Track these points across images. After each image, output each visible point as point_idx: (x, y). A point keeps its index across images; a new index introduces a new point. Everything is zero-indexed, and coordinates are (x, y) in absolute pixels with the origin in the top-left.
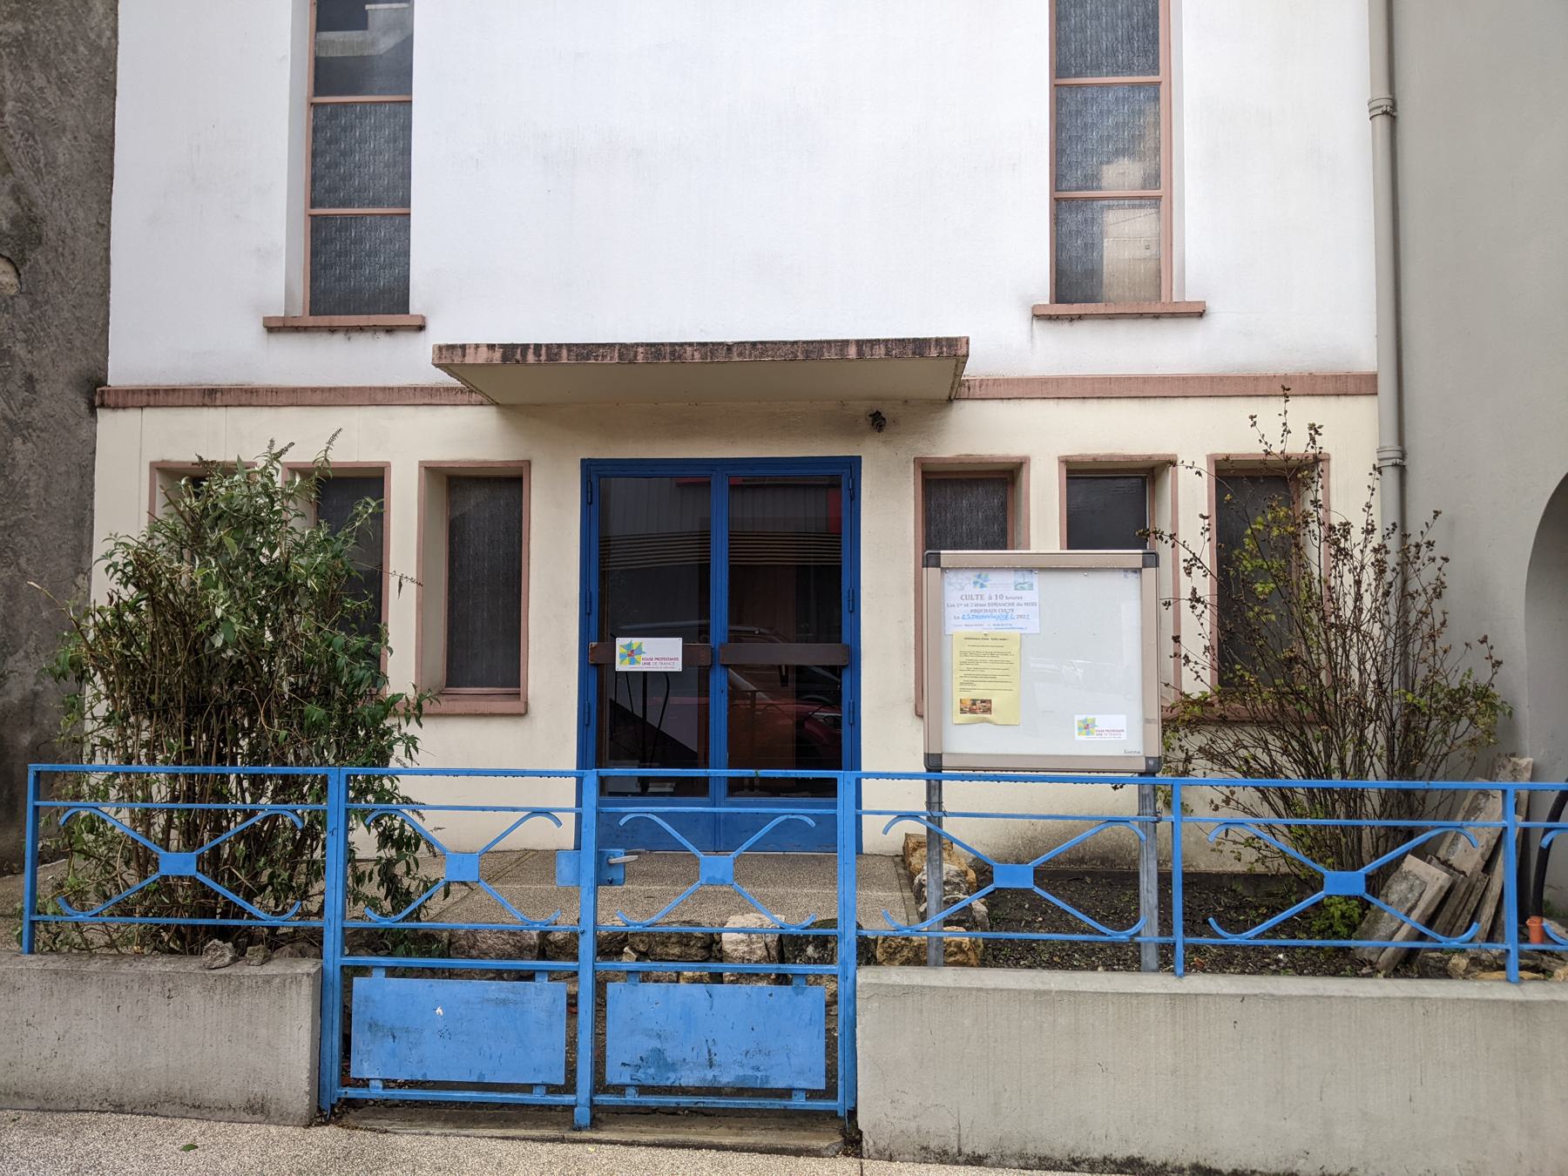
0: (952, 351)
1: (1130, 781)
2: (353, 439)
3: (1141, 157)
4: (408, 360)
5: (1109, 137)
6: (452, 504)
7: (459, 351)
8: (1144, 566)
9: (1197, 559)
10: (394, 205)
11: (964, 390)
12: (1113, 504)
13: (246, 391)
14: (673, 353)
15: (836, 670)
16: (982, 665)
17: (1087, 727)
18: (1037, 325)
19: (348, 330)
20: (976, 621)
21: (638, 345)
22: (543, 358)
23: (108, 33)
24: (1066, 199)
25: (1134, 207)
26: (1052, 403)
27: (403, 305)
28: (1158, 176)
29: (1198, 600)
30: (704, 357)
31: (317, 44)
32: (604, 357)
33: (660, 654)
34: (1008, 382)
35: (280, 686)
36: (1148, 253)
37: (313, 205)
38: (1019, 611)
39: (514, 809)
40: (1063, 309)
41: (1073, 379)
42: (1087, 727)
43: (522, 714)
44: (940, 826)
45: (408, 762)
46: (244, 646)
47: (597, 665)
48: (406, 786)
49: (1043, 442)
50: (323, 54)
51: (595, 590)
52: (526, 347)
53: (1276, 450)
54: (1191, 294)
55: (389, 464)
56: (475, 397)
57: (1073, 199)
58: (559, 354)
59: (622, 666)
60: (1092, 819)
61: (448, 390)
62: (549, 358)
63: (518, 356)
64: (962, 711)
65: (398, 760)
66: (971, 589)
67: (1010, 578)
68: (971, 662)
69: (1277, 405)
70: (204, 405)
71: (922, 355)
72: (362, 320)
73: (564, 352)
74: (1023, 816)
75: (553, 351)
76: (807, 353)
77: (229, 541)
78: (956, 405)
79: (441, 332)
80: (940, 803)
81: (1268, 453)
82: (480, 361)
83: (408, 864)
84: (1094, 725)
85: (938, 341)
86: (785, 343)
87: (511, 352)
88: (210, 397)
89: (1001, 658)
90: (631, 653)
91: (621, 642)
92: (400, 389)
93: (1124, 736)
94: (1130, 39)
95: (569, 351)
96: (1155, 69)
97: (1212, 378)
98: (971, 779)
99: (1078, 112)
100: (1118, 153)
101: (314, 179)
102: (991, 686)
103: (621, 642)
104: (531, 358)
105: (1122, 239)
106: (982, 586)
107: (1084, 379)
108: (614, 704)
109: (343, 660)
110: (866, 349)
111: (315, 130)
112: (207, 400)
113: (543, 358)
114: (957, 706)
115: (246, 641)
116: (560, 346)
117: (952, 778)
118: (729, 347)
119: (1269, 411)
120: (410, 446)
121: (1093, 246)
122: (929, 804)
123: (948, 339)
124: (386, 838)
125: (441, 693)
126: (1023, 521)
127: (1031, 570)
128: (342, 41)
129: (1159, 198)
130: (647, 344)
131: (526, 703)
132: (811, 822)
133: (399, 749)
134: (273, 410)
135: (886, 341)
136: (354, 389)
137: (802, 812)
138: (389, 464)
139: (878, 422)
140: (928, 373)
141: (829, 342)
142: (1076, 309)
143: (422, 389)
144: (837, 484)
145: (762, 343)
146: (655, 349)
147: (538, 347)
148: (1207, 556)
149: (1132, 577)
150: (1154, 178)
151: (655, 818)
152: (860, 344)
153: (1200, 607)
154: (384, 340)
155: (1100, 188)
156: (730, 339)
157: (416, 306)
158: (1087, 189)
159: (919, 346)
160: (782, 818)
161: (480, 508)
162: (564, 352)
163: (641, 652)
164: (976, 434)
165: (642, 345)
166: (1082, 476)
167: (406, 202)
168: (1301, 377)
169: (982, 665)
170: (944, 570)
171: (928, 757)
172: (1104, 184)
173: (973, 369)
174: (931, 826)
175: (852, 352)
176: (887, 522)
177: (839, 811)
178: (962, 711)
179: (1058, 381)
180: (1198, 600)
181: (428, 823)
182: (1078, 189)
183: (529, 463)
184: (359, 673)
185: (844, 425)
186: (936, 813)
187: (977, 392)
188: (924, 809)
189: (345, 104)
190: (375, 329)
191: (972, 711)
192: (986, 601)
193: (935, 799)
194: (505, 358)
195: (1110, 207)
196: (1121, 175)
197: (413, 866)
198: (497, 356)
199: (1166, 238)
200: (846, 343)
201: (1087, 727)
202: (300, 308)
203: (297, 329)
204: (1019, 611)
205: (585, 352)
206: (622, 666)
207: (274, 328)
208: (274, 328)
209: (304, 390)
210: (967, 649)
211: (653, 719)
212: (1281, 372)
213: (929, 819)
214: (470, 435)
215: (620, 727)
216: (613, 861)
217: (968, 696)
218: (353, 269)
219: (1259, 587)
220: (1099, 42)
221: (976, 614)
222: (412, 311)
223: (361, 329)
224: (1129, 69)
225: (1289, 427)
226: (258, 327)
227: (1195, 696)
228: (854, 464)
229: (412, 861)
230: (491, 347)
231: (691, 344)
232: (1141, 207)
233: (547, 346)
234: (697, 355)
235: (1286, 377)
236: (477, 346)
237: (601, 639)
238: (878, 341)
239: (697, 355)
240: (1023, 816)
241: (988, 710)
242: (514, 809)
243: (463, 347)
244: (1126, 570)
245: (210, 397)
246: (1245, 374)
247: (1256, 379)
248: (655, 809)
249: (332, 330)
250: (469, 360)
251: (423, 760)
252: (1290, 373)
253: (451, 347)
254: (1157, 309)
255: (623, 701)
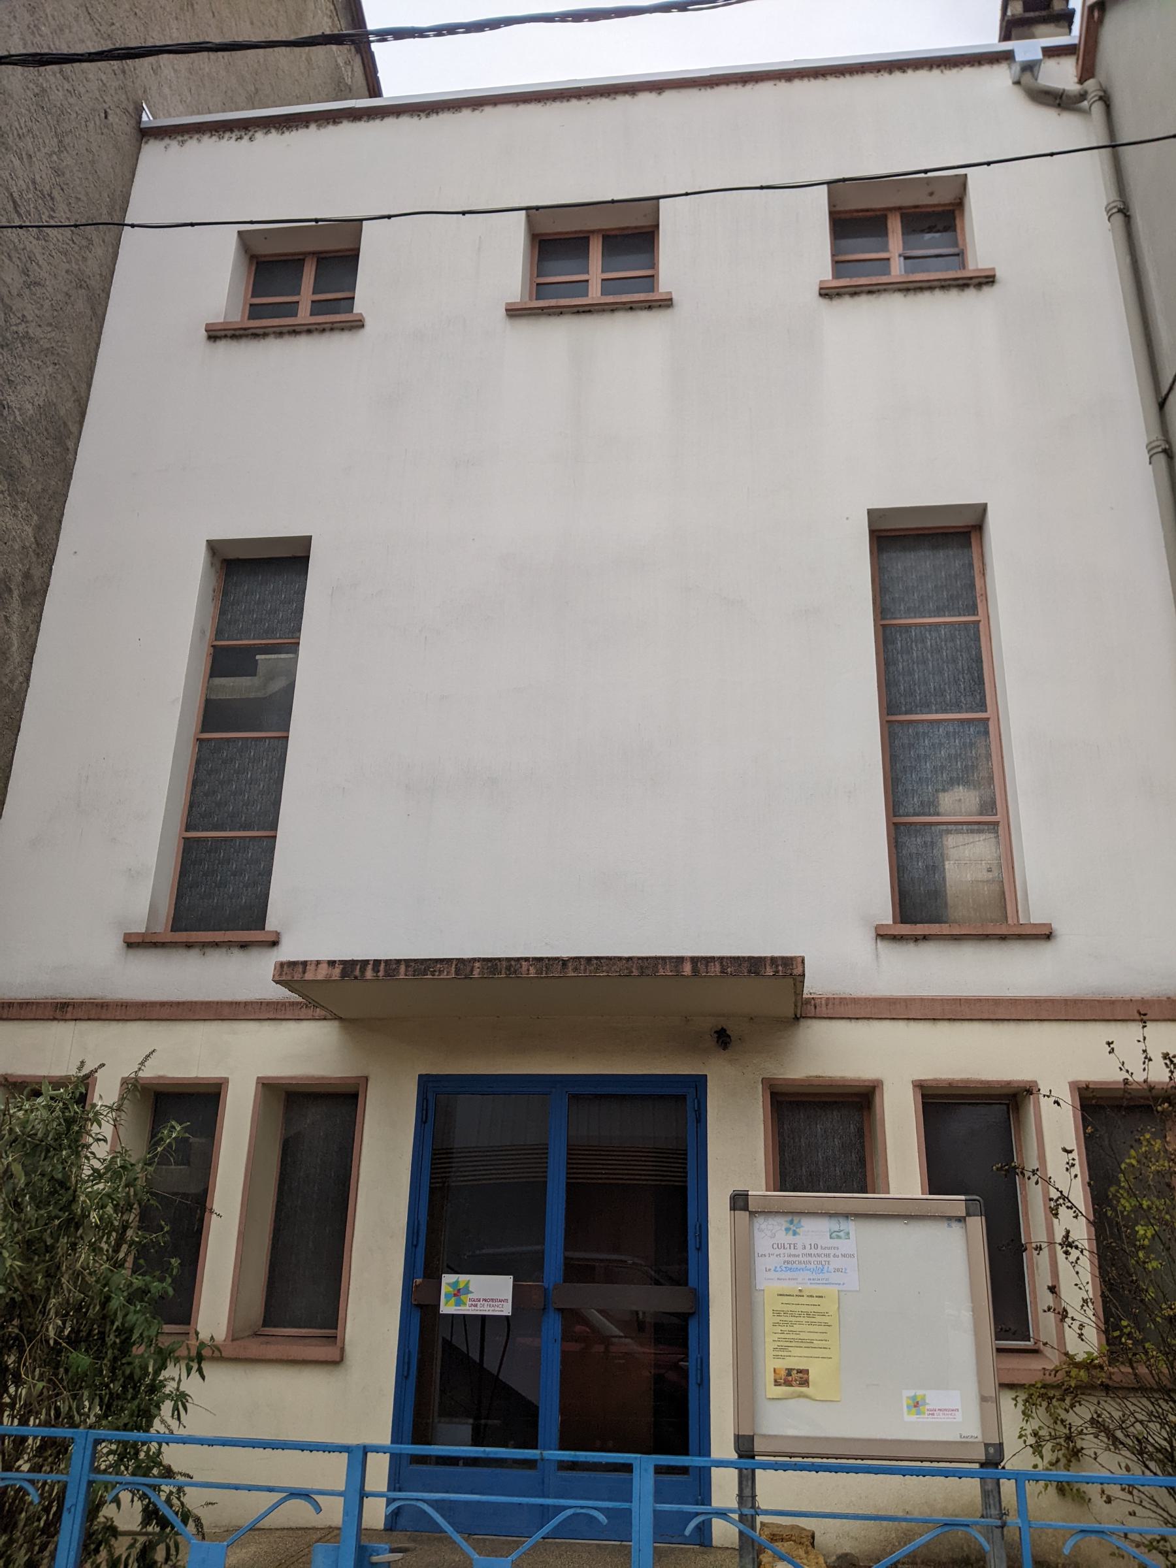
0: (788, 969)
1: (969, 1474)
2: (181, 1054)
3: (976, 785)
4: (250, 975)
5: (943, 767)
6: (288, 1121)
7: (300, 969)
8: (968, 1214)
9: (1064, 1198)
10: (264, 829)
11: (810, 1010)
12: (974, 1133)
13: (97, 1005)
14: (508, 968)
15: (685, 1317)
16: (796, 1328)
17: (917, 1405)
18: (882, 945)
19: (204, 945)
20: (789, 1274)
21: (474, 960)
22: (381, 974)
23: (21, 679)
24: (905, 824)
25: (972, 832)
26: (901, 1024)
27: (259, 921)
28: (994, 803)
29: (1070, 1245)
30: (539, 971)
31: (209, 688)
32: (441, 972)
33: (486, 1294)
34: (855, 1001)
35: (47, 1330)
36: (990, 876)
37: (188, 827)
38: (835, 1263)
39: (270, 1489)
40: (906, 929)
41: (922, 1000)
42: (916, 1404)
43: (337, 1362)
44: (741, 1533)
45: (174, 1424)
46: (17, 1284)
47: (419, 1306)
48: (172, 1456)
49: (897, 1063)
50: (213, 697)
51: (423, 1218)
52: (366, 962)
53: (1139, 1077)
54: (1036, 914)
55: (226, 1080)
56: (319, 1012)
57: (911, 824)
58: (397, 970)
59: (447, 1307)
60: (926, 1521)
61: (293, 1004)
62: (387, 974)
63: (357, 973)
64: (777, 1383)
65: (163, 1422)
66: (783, 1237)
67: (822, 1226)
68: (786, 1323)
69: (1135, 1030)
70: (54, 1019)
71: (757, 974)
72: (218, 936)
73: (403, 968)
74: (856, 1517)
75: (392, 966)
76: (642, 970)
77: (17, 1169)
78: (804, 1023)
79: (288, 951)
80: (754, 1497)
81: (1126, 1082)
82: (320, 977)
83: (168, 1549)
84: (925, 1404)
85: (773, 960)
86: (620, 958)
87: (349, 968)
88: (62, 1010)
89: (818, 1319)
90: (458, 1293)
91: (448, 1279)
92: (246, 1004)
93: (959, 1417)
94: (956, 681)
95: (407, 966)
96: (983, 707)
97: (1066, 1002)
98: (785, 1467)
99: (911, 746)
100: (953, 782)
101: (192, 805)
102: (807, 1352)
103: (448, 1279)
104: (369, 974)
105: (964, 862)
106: (795, 1233)
107: (933, 1000)
108: (447, 1344)
109: (117, 1302)
110: (701, 966)
111: (198, 762)
112: (58, 1014)
113: (381, 974)
114: (770, 1377)
115: (20, 1276)
116: (398, 961)
117: (765, 1466)
118: (564, 962)
119: (1127, 1035)
120: (247, 1060)
121: (935, 868)
122: (741, 1496)
123: (783, 958)
124: (151, 1514)
125: (256, 1335)
126: (880, 1146)
127: (846, 1216)
128: (235, 686)
129: (997, 824)
130: (484, 960)
131: (343, 1350)
132: (602, 1518)
133: (167, 1407)
134: (120, 1025)
135: (721, 959)
136: (202, 1003)
137: (595, 1508)
138: (226, 1080)
139: (723, 1039)
140: (759, 997)
141: (664, 959)
142: (920, 929)
143: (268, 1004)
144: (684, 1100)
145: (597, 958)
146: (492, 965)
147: (377, 962)
148: (1079, 1195)
149: (957, 1228)
150: (989, 806)
151: (425, 1507)
152: (695, 960)
153: (1075, 1253)
154: (237, 956)
155: (938, 814)
156: (565, 954)
157: (272, 924)
158: (924, 814)
159: (754, 965)
160: (569, 1512)
161: (313, 1125)
162: (403, 968)
163: (468, 1292)
164: (832, 1053)
165: (479, 960)
166: (940, 1104)
167: (274, 826)
168: (1159, 1002)
169: (796, 1328)
170: (753, 1214)
171: (738, 1438)
172: (941, 810)
173: (814, 985)
174: (742, 1527)
175: (687, 969)
176: (736, 1151)
177: (635, 1506)
178: (777, 1383)
179: (907, 1002)
180: (1070, 1245)
181: (193, 1499)
182: (915, 814)
183: (367, 1079)
184: (132, 1318)
185: (684, 1040)
186: (746, 1511)
187: (823, 1011)
188: (734, 1504)
189: (228, 740)
190: (229, 945)
191: (788, 1383)
192: (800, 1251)
193: (747, 1492)
194: (344, 974)
195: (949, 832)
196: (957, 802)
197: (173, 1551)
198: (337, 972)
199: (1007, 861)
200: (680, 960)
201: (917, 1405)
202: (162, 927)
203: (156, 945)
204: (835, 1263)
205: (422, 967)
206: (447, 1307)
207: (134, 943)
208: (134, 943)
209: (153, 1004)
210: (779, 1307)
211: (491, 1364)
212: (1138, 996)
213: (741, 1516)
214: (305, 1049)
215: (448, 1380)
216: (375, 1559)
217: (783, 1365)
218: (218, 881)
219: (1140, 1230)
220: (926, 683)
221: (789, 1266)
222: (267, 928)
223: (216, 945)
224: (958, 707)
225: (1150, 1054)
226: (119, 942)
227: (1078, 1359)
228: (699, 1083)
229: (172, 1544)
230: (332, 963)
231: (527, 959)
232: (979, 831)
233: (387, 961)
234: (532, 970)
235: (1143, 1001)
236: (318, 963)
237: (427, 1275)
238: (713, 958)
239: (532, 970)
240: (856, 1517)
241: (805, 1383)
242: (270, 1489)
243: (305, 964)
244: (950, 1218)
245: (62, 1010)
246: (1100, 997)
247: (1112, 1003)
248: (426, 1495)
249: (189, 946)
250: (309, 976)
251: (194, 1423)
252: (1147, 996)
253: (293, 964)
254: (1003, 930)
255: (458, 1342)
